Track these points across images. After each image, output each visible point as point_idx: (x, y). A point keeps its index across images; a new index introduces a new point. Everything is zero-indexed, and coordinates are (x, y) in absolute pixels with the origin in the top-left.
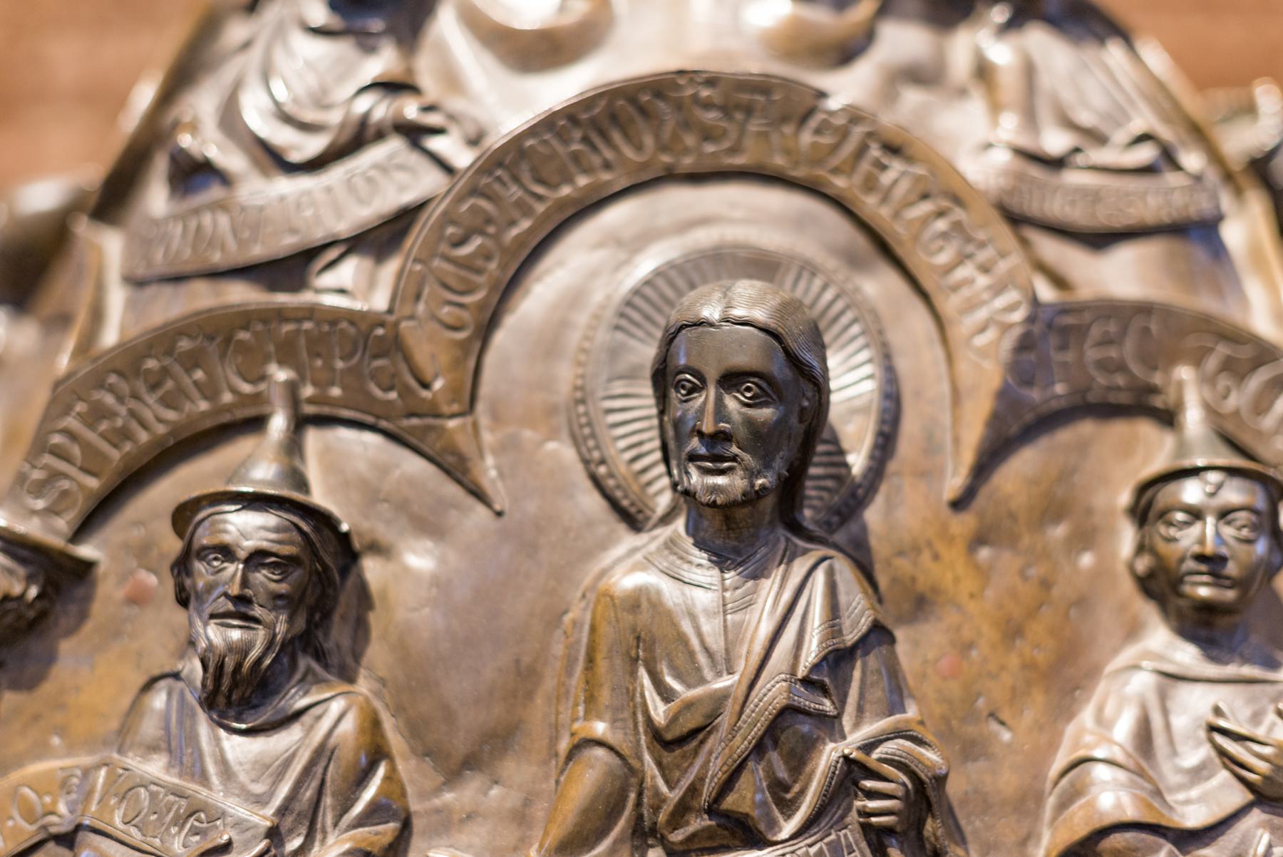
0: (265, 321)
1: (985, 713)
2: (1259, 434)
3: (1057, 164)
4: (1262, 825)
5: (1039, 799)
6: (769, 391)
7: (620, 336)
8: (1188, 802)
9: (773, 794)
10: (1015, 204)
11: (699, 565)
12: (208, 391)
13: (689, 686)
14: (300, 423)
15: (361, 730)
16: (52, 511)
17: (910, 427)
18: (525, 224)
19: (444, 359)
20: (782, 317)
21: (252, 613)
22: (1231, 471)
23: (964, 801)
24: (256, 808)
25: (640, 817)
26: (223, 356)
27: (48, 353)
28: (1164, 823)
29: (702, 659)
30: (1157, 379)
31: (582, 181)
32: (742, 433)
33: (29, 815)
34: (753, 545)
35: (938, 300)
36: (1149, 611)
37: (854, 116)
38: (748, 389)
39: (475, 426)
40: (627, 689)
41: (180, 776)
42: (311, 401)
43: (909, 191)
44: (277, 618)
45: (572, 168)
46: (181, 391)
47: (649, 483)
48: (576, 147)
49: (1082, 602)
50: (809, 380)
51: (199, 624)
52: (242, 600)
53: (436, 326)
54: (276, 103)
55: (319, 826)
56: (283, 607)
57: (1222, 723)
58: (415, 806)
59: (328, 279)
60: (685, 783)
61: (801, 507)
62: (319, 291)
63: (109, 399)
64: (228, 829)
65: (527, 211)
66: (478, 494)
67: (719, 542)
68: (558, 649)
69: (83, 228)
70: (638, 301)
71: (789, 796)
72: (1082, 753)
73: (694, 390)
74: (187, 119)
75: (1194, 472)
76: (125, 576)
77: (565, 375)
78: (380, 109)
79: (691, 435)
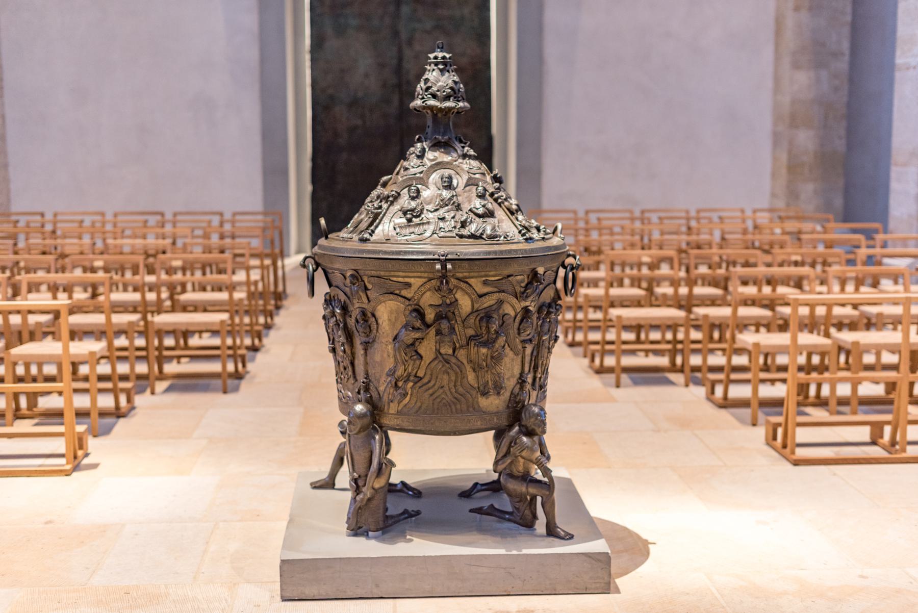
78: (421, 164)
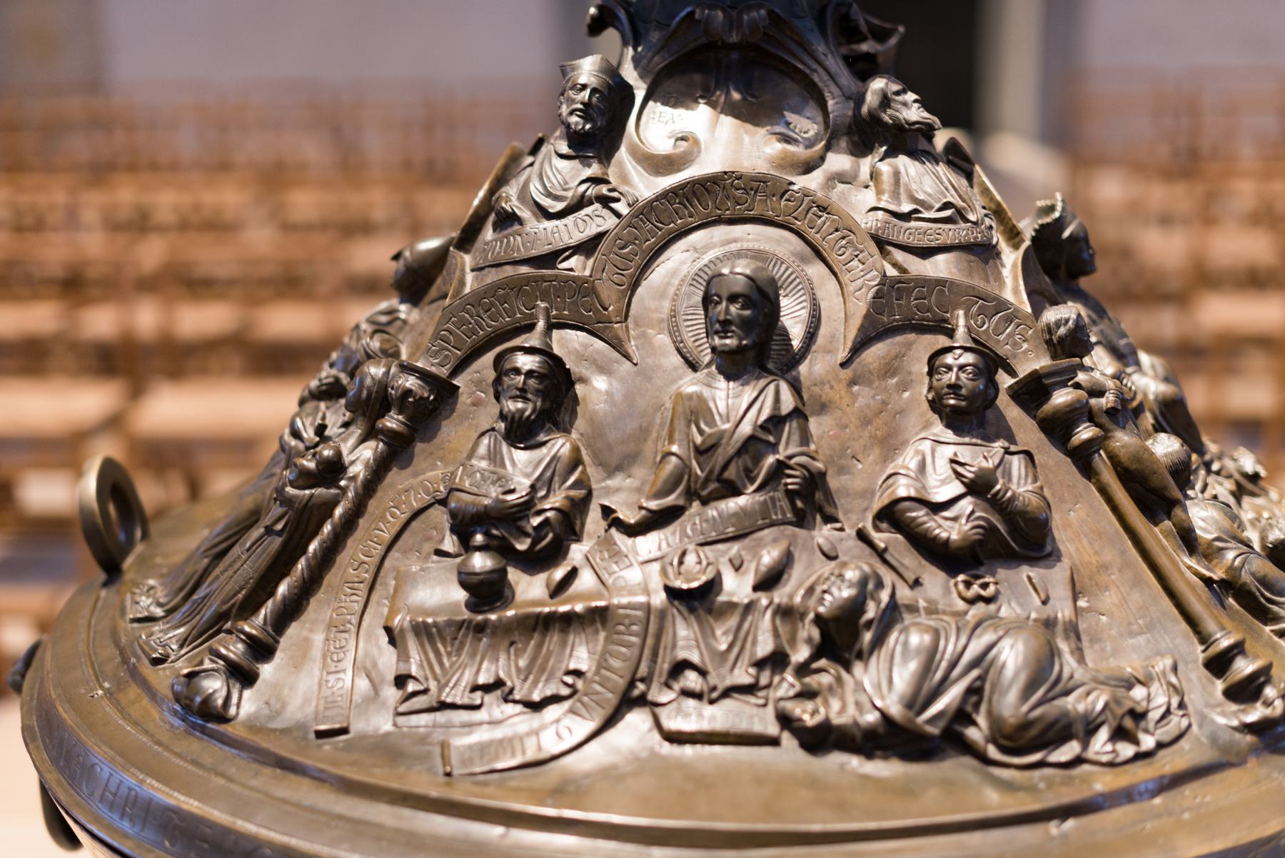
3: (905, 217)
4: (971, 503)
7: (692, 288)
12: (511, 313)
14: (550, 327)
17: (823, 331)
19: (614, 297)
28: (924, 498)
29: (717, 417)
32: (737, 321)
33: (427, 492)
37: (806, 193)
39: (627, 327)
47: (702, 351)
49: (901, 412)
58: (594, 486)
60: (707, 469)
66: (627, 357)
68: (658, 421)
73: (718, 303)
75: (949, 349)
77: (667, 305)
78: (592, 191)
79: (715, 323)
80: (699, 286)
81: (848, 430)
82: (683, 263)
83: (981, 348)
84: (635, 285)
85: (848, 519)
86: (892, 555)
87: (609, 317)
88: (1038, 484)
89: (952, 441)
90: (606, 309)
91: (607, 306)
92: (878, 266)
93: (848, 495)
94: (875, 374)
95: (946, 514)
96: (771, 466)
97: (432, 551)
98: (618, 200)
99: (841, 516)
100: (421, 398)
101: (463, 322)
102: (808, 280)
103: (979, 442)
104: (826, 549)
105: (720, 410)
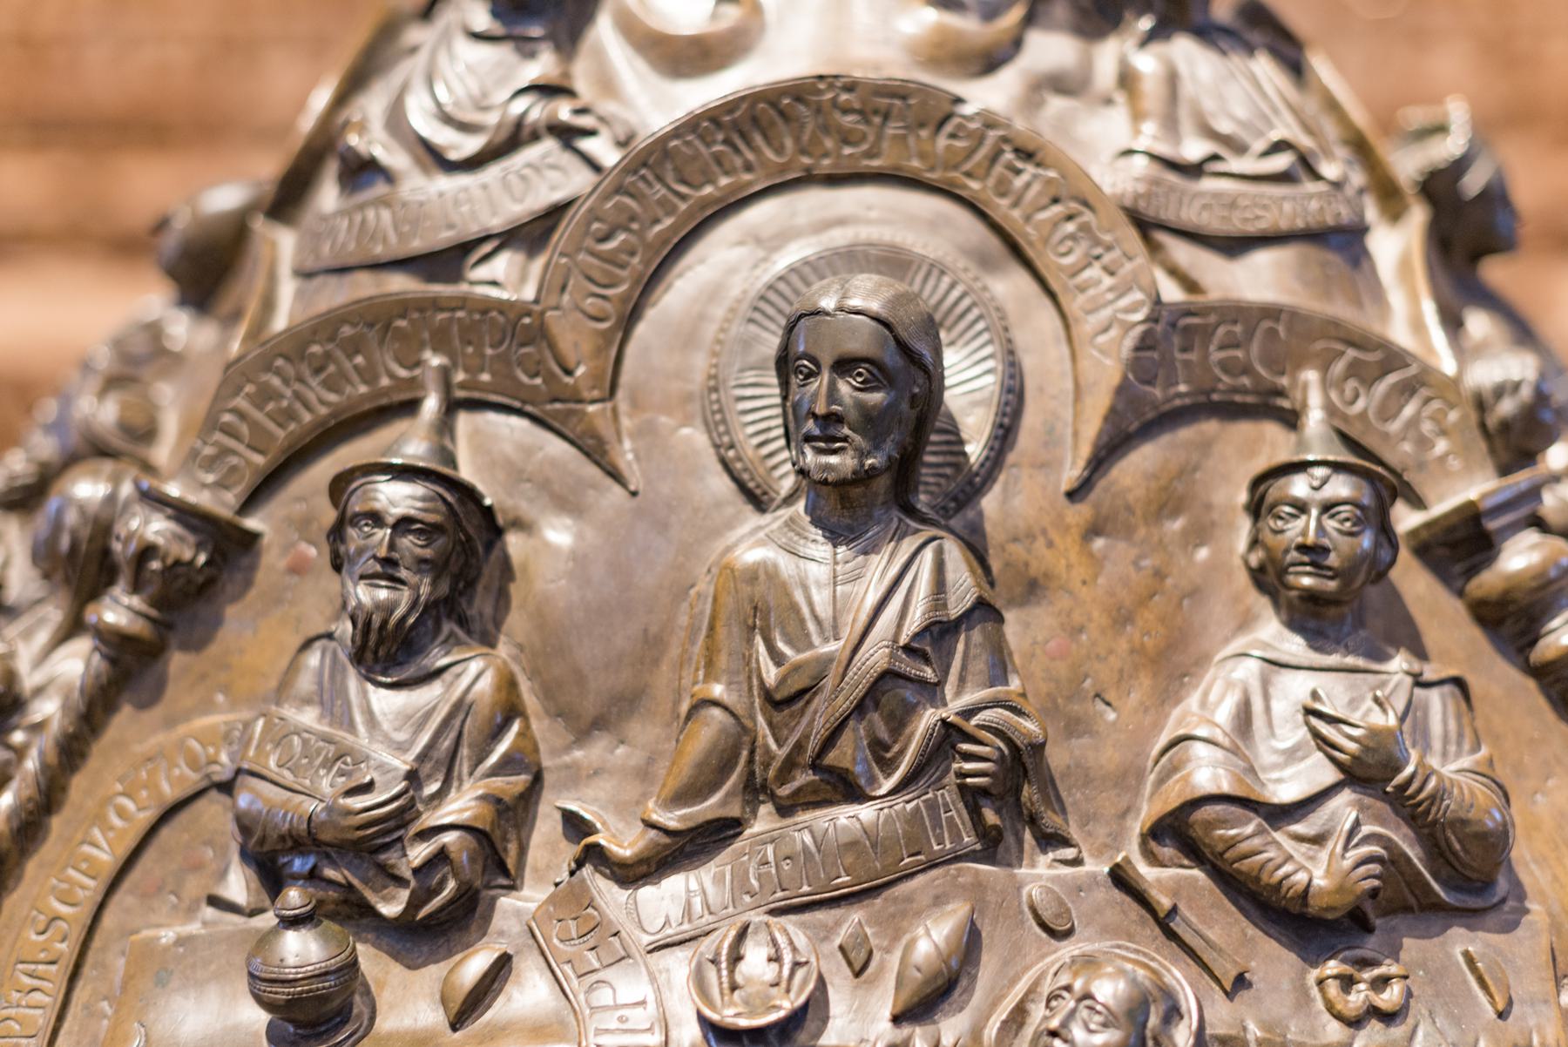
0: (421, 310)
1: (1092, 694)
2: (1386, 436)
3: (1193, 170)
4: (1352, 804)
5: (1140, 776)
6: (880, 377)
7: (752, 328)
8: (1279, 781)
9: (874, 753)
10: (1150, 211)
11: (814, 541)
12: (368, 375)
13: (798, 651)
14: (452, 406)
15: (498, 688)
16: (221, 485)
17: (1031, 419)
18: (668, 222)
19: (587, 347)
20: (894, 308)
21: (398, 575)
22: (1337, 467)
23: (1067, 774)
24: (397, 753)
25: (752, 774)
26: (382, 342)
27: (223, 344)
28: (1253, 797)
29: (811, 626)
30: (1284, 381)
31: (724, 181)
32: (853, 415)
33: (194, 764)
34: (866, 523)
35: (1062, 299)
36: (1263, 604)
37: (989, 121)
38: (860, 374)
39: (615, 411)
40: (744, 655)
41: (331, 725)
42: (462, 386)
43: (1040, 194)
44: (421, 581)
45: (716, 169)
46: (342, 375)
47: (775, 467)
48: (718, 148)
49: (1194, 593)
50: (920, 368)
51: (350, 584)
52: (388, 562)
53: (580, 316)
54: (438, 105)
55: (456, 774)
56: (428, 571)
57: (1318, 706)
58: (546, 762)
59: (482, 272)
60: (792, 741)
61: (916, 491)
62: (472, 283)
63: (276, 382)
64: (371, 771)
65: (671, 210)
66: (615, 475)
67: (834, 520)
68: (683, 620)
69: (259, 224)
70: (772, 296)
71: (888, 755)
72: (1181, 732)
73: (810, 375)
74: (356, 118)
75: (1301, 467)
76: (288, 547)
77: (700, 363)
78: (536, 111)
79: (806, 419)
80: (773, 327)
81: (1084, 637)
82: (732, 270)
83: (1367, 464)
84: (631, 317)
85: (1090, 834)
86: (1188, 924)
87: (575, 389)
88: (1484, 751)
89: (1306, 663)
90: (569, 372)
91: (571, 364)
92: (1145, 281)
93: (1087, 780)
94: (1139, 512)
95: (1299, 828)
96: (929, 736)
97: (204, 896)
98: (590, 133)
99: (1074, 832)
100: (178, 563)
101: (265, 395)
102: (998, 309)
103: (1360, 662)
104: (1046, 915)
105: (819, 610)
